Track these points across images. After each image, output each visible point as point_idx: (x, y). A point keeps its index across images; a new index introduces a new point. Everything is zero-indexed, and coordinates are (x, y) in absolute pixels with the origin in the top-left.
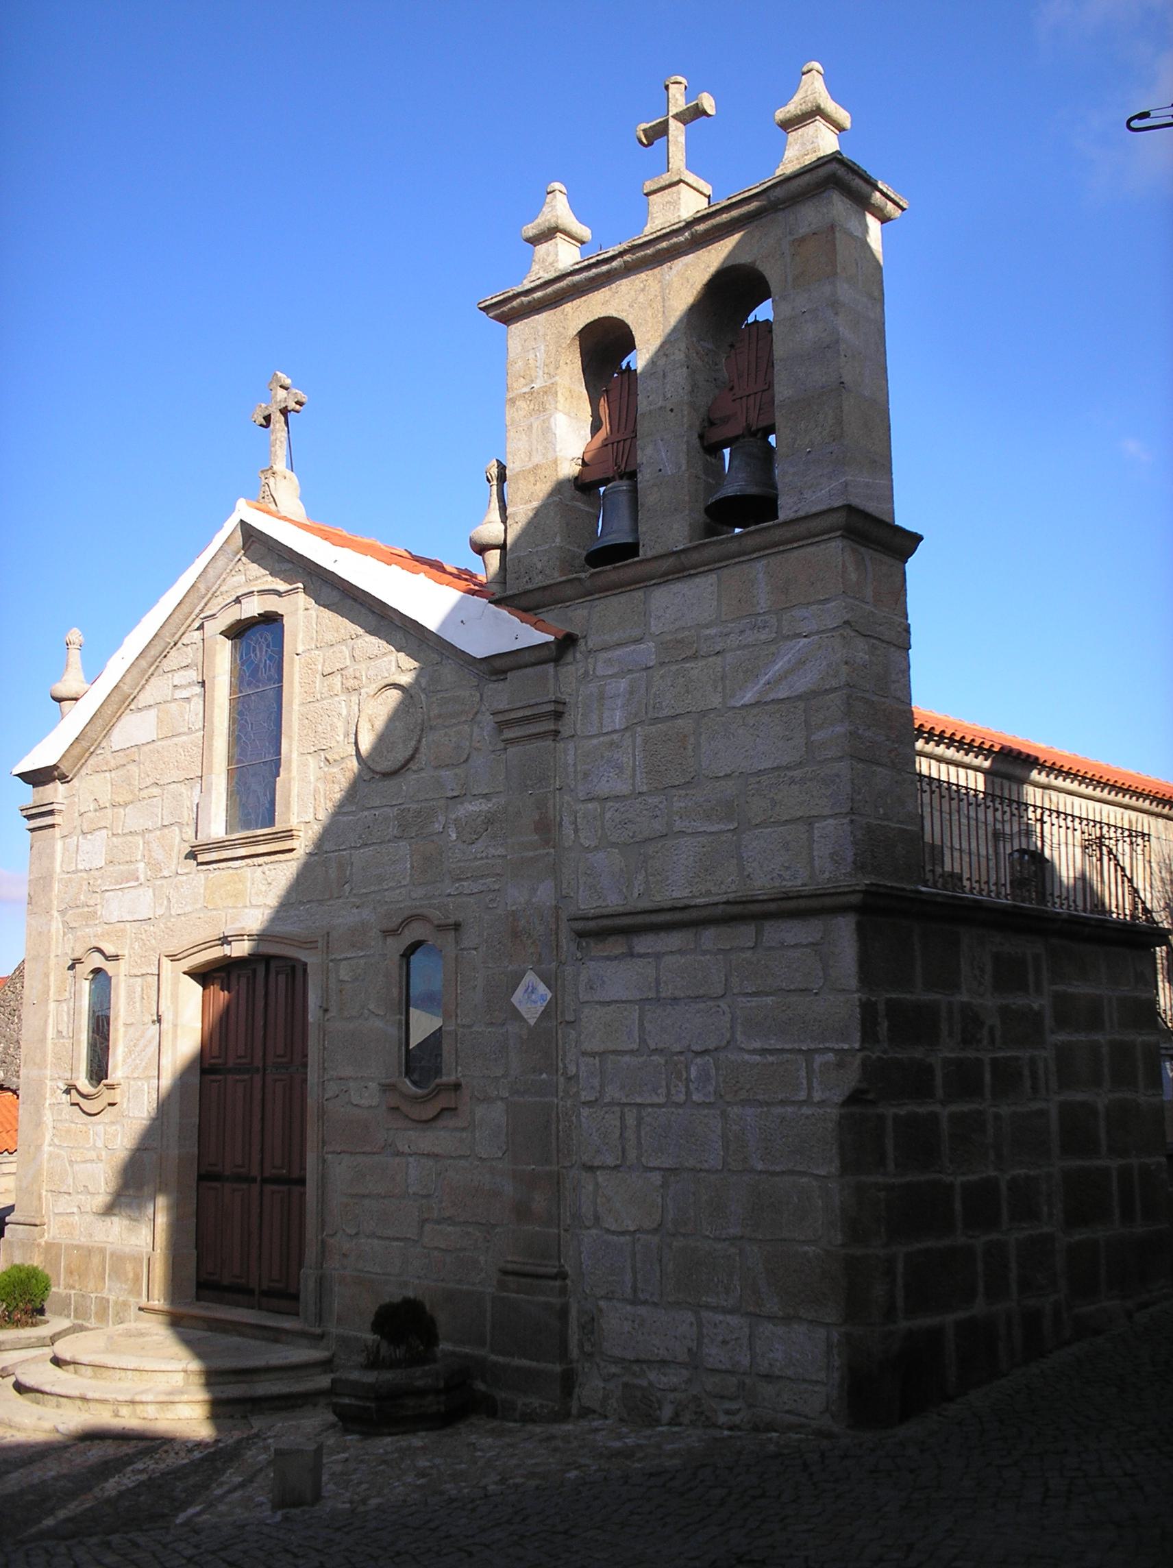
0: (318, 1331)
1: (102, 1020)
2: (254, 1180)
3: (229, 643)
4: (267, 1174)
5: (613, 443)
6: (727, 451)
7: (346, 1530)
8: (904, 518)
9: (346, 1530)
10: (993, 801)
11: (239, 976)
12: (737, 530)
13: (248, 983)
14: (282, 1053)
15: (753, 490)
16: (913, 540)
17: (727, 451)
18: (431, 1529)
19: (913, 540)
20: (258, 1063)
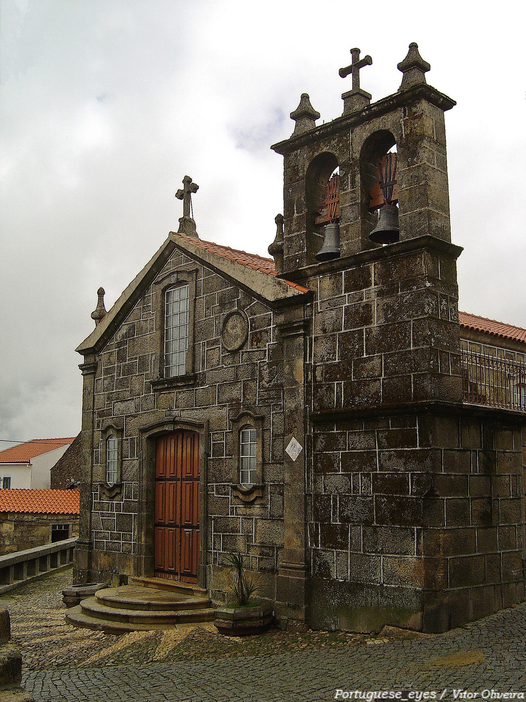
0: (204, 590)
1: (335, 500)
2: (177, 526)
3: (294, 122)
4: (183, 524)
5: (330, 204)
6: (379, 210)
7: (211, 666)
8: (455, 241)
9: (211, 666)
10: (505, 366)
11: (187, 438)
12: (384, 245)
13: (191, 442)
14: (189, 472)
15: (389, 228)
16: (459, 250)
17: (379, 210)
18: (245, 667)
19: (459, 250)
20: (179, 476)
